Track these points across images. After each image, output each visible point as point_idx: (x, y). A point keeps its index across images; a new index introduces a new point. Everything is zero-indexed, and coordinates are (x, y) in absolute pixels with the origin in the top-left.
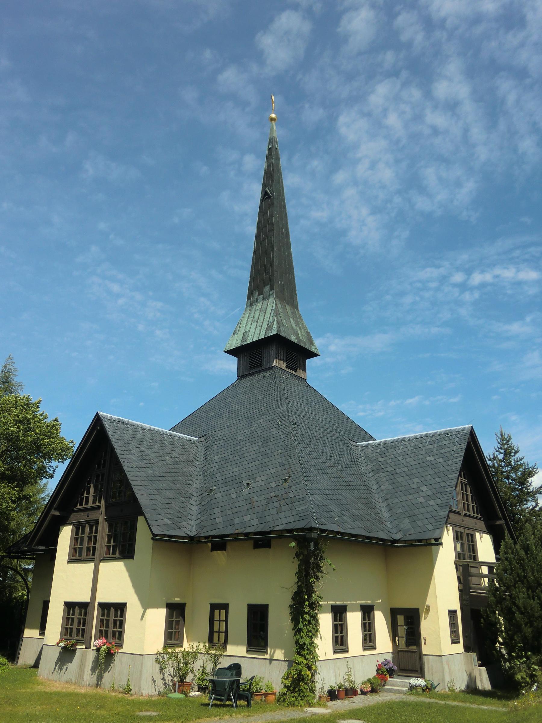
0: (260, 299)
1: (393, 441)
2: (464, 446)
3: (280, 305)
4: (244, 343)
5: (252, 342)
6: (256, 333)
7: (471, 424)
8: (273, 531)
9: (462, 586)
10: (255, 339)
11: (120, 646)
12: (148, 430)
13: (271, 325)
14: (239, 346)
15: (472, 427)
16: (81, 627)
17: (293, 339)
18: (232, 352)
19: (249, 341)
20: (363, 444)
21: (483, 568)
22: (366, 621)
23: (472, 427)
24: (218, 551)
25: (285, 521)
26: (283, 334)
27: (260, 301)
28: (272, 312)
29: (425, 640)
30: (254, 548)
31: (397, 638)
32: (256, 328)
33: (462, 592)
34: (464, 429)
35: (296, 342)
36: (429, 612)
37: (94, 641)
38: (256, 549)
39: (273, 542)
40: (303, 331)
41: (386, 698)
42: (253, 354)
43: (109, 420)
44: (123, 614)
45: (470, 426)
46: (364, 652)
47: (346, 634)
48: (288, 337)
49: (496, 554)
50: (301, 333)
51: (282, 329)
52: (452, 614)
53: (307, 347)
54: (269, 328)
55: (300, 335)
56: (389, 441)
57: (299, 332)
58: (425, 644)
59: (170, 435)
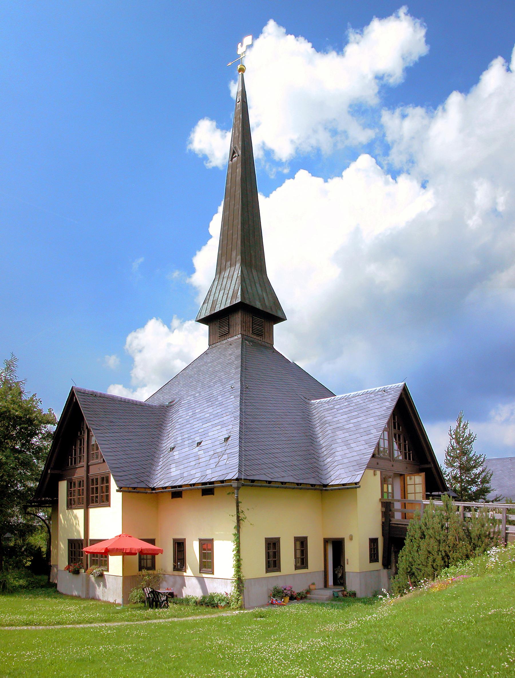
3: (246, 271)
4: (213, 312)
5: (220, 311)
6: (222, 301)
8: (197, 483)
9: (384, 520)
10: (223, 308)
11: (108, 570)
12: (119, 401)
14: (208, 315)
16: (73, 557)
18: (205, 321)
19: (217, 310)
25: (197, 475)
26: (247, 302)
27: (228, 268)
29: (347, 561)
30: (202, 496)
32: (228, 294)
33: (384, 525)
35: (261, 308)
37: (90, 567)
38: (204, 496)
39: (216, 491)
40: (269, 296)
42: (223, 322)
43: (83, 393)
44: (296, 566)
46: (297, 570)
48: (252, 304)
50: (268, 298)
51: (246, 296)
52: (373, 542)
53: (274, 313)
54: (234, 296)
55: (266, 301)
58: (348, 563)
59: (140, 405)
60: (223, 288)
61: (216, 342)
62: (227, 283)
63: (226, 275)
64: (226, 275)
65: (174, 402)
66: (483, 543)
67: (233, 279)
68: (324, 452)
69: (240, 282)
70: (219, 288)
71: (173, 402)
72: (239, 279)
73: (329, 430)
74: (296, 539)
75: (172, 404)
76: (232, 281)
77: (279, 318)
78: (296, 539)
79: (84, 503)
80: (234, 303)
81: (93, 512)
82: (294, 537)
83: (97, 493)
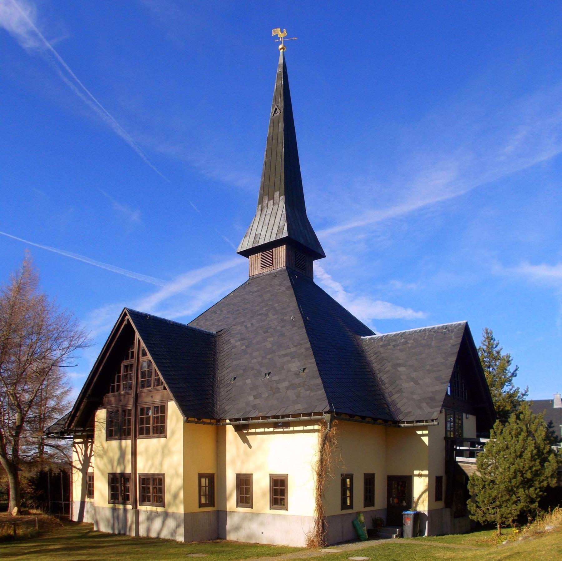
0: (270, 204)
1: (395, 335)
2: (460, 340)
4: (256, 245)
5: (264, 244)
7: (465, 320)
10: (267, 241)
12: (171, 324)
13: (281, 229)
15: (467, 324)
17: (302, 242)
20: (367, 338)
21: (7, 496)
22: (280, 488)
23: (467, 324)
24: (452, 370)
28: (282, 217)
31: (391, 498)
34: (460, 324)
36: (93, 494)
41: (505, 555)
45: (465, 321)
47: (238, 496)
49: (477, 431)
54: (280, 230)
56: (391, 335)
57: (307, 235)
60: (266, 224)
61: (258, 273)
62: (271, 219)
63: (269, 212)
64: (269, 212)
65: (223, 332)
66: (505, 450)
67: (277, 216)
68: (388, 388)
69: (286, 219)
70: (261, 222)
71: (222, 331)
72: (284, 217)
73: (388, 366)
74: (366, 475)
75: (220, 333)
76: (276, 218)
77: (320, 255)
78: (366, 475)
79: (129, 550)
80: (281, 238)
81: (142, 444)
82: (365, 474)
83: (142, 381)
